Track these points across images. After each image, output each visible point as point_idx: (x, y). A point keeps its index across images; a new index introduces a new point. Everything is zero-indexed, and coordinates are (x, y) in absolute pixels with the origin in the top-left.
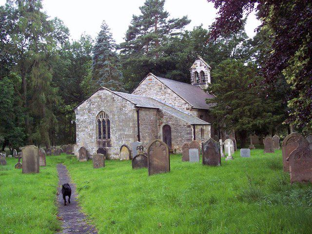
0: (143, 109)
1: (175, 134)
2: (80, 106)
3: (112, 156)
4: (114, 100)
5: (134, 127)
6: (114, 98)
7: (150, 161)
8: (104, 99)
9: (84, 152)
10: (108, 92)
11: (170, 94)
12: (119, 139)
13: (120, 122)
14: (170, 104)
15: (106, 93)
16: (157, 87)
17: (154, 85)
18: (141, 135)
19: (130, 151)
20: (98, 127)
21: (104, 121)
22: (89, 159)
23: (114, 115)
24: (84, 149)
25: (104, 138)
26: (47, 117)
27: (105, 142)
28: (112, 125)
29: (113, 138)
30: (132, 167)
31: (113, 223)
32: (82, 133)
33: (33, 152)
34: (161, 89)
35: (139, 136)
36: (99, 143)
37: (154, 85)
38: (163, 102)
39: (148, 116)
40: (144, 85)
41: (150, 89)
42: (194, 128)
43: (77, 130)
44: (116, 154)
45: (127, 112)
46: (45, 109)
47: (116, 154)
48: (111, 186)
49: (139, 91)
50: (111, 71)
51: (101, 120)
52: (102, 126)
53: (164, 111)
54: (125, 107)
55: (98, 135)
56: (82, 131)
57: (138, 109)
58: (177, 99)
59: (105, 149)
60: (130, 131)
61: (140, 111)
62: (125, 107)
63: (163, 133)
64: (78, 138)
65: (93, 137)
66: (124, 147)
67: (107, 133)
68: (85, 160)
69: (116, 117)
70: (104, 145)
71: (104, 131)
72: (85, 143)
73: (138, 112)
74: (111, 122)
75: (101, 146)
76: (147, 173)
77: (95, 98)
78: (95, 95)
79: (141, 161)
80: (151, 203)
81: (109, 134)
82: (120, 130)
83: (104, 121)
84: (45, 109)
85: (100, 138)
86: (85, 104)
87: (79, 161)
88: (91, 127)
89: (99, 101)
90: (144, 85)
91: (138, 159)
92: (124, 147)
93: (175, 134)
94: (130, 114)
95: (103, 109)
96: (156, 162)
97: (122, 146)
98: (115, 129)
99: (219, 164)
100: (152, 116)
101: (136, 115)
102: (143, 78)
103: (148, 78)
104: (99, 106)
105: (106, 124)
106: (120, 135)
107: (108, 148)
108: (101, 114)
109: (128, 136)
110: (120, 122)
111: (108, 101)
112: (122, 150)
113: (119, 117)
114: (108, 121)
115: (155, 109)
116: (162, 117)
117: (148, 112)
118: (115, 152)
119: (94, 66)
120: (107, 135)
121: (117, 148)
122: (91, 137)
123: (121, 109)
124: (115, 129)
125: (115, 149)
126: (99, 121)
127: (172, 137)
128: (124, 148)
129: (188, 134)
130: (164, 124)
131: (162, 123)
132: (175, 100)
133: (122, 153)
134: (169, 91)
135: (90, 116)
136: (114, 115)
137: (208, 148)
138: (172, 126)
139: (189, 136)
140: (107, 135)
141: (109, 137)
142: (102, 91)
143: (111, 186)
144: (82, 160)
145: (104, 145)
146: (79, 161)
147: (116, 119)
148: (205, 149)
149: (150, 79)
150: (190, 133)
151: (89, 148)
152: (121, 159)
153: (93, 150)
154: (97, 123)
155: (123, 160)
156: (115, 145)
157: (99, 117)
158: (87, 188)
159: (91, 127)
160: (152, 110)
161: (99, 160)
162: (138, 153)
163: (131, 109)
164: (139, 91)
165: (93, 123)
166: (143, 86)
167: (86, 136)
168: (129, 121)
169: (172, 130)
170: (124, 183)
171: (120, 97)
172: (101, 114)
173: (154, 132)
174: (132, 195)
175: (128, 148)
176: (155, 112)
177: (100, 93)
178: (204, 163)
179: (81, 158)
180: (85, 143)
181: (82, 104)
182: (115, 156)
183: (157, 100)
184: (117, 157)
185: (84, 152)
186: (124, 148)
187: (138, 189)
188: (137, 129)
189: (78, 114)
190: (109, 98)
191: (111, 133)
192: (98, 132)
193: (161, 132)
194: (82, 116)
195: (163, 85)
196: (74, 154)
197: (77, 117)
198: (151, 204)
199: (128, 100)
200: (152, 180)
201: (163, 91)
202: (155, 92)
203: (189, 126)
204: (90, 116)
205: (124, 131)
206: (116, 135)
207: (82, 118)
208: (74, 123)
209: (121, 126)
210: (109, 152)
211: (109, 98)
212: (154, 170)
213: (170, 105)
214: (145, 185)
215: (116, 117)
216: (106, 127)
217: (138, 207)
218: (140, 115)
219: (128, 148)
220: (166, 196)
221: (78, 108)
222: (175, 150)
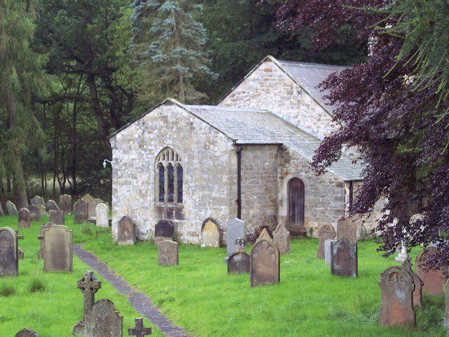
0: (250, 148)
1: (312, 197)
2: (123, 132)
3: (186, 238)
4: (192, 128)
5: (231, 184)
6: (192, 124)
7: (254, 268)
8: (173, 123)
9: (129, 226)
10: (181, 110)
11: (308, 106)
12: (200, 205)
13: (203, 171)
14: (309, 127)
15: (175, 110)
16: (281, 88)
17: (276, 84)
18: (243, 199)
19: (221, 231)
20: (158, 178)
21: (170, 167)
22: (138, 240)
23: (191, 157)
24: (130, 220)
25: (171, 200)
26: (21, 125)
27: (171, 209)
28: (186, 177)
29: (188, 202)
30: (225, 267)
31: (215, 332)
32: (124, 187)
33: (62, 236)
34: (291, 93)
35: (239, 201)
36: (159, 210)
37: (276, 84)
38: (293, 122)
39: (258, 161)
40: (254, 80)
41: (268, 92)
42: (351, 188)
43: (114, 180)
44: (193, 234)
45: (217, 154)
46: (16, 106)
47: (193, 234)
48: (202, 299)
49: (244, 93)
50: (178, 23)
51: (165, 164)
52: (166, 177)
53: (292, 149)
54: (214, 143)
55: (158, 193)
56: (125, 183)
57: (240, 149)
58: (323, 118)
59: (172, 223)
60: (223, 191)
61: (243, 152)
62: (214, 143)
63: (289, 194)
64: (117, 197)
65: (148, 198)
66: (209, 222)
67: (175, 191)
68: (131, 242)
69: (196, 161)
70: (169, 214)
71: (171, 186)
72: (129, 208)
73: (239, 154)
74: (185, 170)
75: (164, 218)
76: (248, 283)
77: (155, 119)
78: (154, 113)
79: (242, 262)
80: (249, 318)
81: (180, 194)
82: (203, 188)
83: (170, 167)
84: (16, 106)
85: (162, 200)
86: (133, 130)
87: (117, 244)
88: (145, 177)
89: (161, 128)
90: (254, 80)
91: (237, 258)
92: (209, 222)
93: (312, 197)
94: (224, 159)
95: (169, 142)
96: (262, 269)
97: (206, 221)
98: (192, 185)
99: (354, 275)
100: (266, 160)
101: (234, 160)
102: (255, 62)
103: (263, 66)
104: (162, 137)
105: (175, 173)
106: (203, 197)
107: (177, 221)
108: (165, 152)
109: (218, 201)
110: (203, 171)
111: (179, 129)
112: (206, 227)
113: (201, 163)
114: (180, 169)
115: (272, 144)
116: (287, 161)
117: (258, 153)
118: (192, 230)
119: (138, 11)
120: (175, 196)
121: (196, 223)
122: (143, 196)
123: (205, 146)
124: (192, 185)
125: (192, 225)
126: (161, 168)
127: (306, 204)
128: (210, 224)
129: (337, 199)
130: (290, 177)
131: (287, 173)
132: (319, 120)
133: (205, 233)
134: (307, 99)
135: (142, 155)
136: (191, 157)
137: (339, 250)
138: (306, 182)
139: (339, 203)
140: (175, 196)
141: (180, 200)
142: (168, 107)
143: (202, 299)
144: (123, 243)
145: (169, 214)
146: (117, 244)
147: (195, 166)
148: (335, 252)
149: (267, 70)
150: (343, 199)
151: (138, 219)
152: (203, 245)
153: (148, 224)
154: (157, 171)
155: (207, 248)
156: (192, 216)
157: (162, 158)
158: (172, 300)
159: (145, 177)
160: (267, 147)
161: (168, 252)
162: (237, 250)
163: (225, 149)
164: (244, 93)
165: (149, 169)
166: (251, 83)
167: (134, 194)
168: (221, 172)
169: (307, 189)
170: (219, 297)
171: (205, 123)
172: (165, 152)
173: (271, 191)
174: (228, 311)
175: (218, 225)
176: (274, 151)
177: (164, 109)
178: (333, 271)
179: (121, 237)
180: (129, 208)
181: (126, 129)
182: (190, 239)
183: (281, 116)
184: (195, 240)
185: (129, 226)
186: (210, 224)
187: (237, 304)
188: (235, 188)
189: (116, 148)
190: (182, 123)
191: (184, 193)
192: (158, 189)
193: (284, 192)
194: (125, 152)
195: (294, 85)
196: (94, 222)
197: (115, 154)
198: (248, 318)
199: (222, 129)
200: (253, 294)
201: (295, 98)
202: (278, 98)
203: (340, 185)
204: (142, 155)
205: (211, 190)
206: (194, 197)
207: (125, 158)
208: (109, 165)
209: (205, 180)
210: (179, 230)
211: (182, 123)
212: (258, 279)
213: (309, 131)
214: (244, 300)
215: (196, 161)
216: (176, 179)
217: (236, 320)
218: (242, 159)
219: (218, 225)
220: (263, 312)
221: (119, 136)
222: (311, 231)
